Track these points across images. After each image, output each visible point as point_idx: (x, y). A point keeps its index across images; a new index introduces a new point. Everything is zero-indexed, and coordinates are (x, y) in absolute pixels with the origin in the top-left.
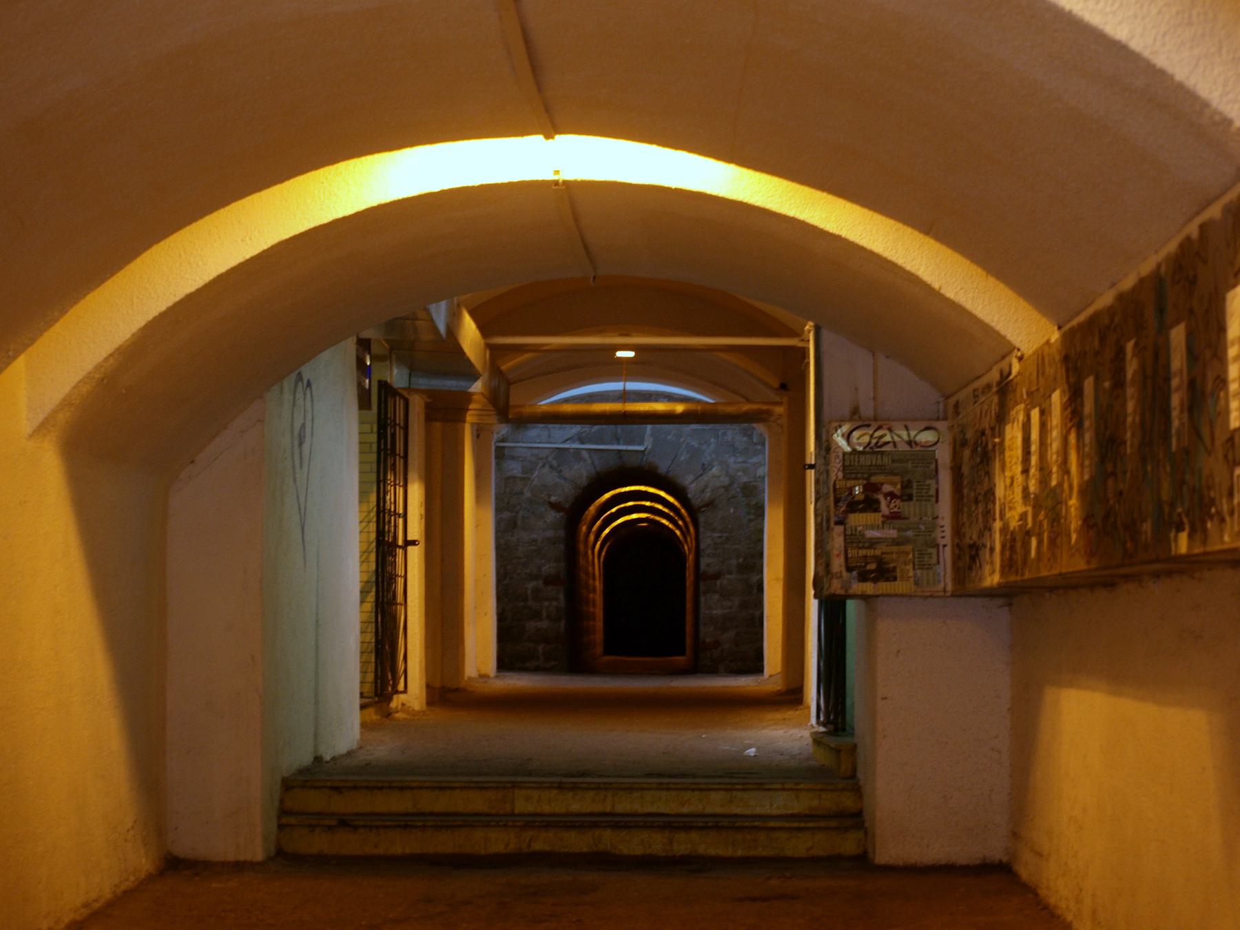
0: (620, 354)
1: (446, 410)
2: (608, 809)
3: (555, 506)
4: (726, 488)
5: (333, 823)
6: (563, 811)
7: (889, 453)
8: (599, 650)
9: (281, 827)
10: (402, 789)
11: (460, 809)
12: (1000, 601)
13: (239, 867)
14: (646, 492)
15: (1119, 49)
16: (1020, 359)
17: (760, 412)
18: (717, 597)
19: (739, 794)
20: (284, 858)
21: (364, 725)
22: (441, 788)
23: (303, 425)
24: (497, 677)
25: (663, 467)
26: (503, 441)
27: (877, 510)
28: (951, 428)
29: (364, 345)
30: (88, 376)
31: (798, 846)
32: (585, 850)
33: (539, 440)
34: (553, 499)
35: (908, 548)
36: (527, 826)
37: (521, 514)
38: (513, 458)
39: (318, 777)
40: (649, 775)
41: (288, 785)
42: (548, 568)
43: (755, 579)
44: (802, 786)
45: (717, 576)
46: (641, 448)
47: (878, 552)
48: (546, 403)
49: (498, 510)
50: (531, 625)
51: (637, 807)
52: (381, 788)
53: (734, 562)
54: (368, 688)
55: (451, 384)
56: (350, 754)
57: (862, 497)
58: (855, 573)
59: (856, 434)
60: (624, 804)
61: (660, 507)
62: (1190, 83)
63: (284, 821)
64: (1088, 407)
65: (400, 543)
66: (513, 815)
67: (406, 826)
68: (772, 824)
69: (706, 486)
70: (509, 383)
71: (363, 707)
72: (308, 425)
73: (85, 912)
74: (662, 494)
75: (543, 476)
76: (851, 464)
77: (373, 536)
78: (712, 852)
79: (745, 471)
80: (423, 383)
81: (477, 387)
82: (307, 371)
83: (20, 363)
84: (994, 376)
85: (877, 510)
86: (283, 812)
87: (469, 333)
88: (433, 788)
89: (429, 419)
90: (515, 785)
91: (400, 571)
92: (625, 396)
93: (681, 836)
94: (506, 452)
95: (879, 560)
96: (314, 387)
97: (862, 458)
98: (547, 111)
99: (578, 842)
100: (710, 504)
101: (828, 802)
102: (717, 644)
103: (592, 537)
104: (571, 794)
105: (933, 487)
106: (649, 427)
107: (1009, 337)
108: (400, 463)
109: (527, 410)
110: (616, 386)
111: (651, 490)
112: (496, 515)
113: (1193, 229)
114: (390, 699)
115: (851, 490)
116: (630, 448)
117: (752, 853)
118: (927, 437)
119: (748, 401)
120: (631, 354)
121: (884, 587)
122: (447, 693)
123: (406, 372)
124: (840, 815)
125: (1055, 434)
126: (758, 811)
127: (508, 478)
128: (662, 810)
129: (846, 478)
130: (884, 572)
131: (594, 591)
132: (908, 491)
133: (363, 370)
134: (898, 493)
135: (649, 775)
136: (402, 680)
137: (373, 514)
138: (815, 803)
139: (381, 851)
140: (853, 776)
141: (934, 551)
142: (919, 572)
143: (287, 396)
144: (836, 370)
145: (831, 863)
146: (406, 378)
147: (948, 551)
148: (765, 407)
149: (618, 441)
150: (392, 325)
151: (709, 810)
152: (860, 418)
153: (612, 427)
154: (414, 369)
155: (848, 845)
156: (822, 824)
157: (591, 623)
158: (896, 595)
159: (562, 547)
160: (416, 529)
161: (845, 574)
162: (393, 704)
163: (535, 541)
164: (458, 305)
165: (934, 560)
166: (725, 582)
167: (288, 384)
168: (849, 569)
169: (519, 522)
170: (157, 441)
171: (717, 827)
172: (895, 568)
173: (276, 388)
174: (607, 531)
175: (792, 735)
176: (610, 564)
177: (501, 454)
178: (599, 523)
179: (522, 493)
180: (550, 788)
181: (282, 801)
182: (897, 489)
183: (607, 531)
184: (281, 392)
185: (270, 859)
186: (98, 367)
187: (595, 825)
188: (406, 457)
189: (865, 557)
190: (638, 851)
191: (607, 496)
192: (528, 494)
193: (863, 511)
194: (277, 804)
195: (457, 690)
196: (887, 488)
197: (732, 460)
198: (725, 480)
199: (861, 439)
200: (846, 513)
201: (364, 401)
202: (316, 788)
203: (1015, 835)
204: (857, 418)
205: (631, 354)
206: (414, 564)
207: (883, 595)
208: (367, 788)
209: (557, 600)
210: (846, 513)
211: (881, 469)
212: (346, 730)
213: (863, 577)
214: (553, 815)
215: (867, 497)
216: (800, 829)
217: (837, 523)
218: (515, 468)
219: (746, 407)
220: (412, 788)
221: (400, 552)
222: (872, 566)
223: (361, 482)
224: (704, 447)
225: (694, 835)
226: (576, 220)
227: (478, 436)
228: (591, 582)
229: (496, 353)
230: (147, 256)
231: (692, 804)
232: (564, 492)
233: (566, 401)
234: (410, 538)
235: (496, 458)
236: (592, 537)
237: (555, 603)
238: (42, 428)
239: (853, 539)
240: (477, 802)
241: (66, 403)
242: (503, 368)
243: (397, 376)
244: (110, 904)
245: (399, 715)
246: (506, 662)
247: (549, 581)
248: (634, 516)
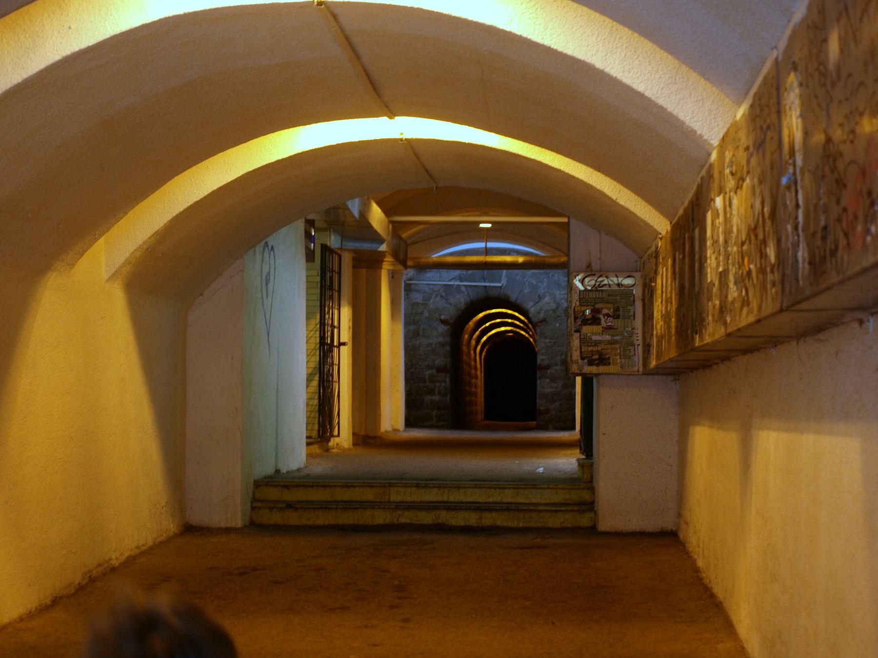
0: (482, 225)
1: (368, 263)
2: (445, 499)
3: (444, 322)
4: (554, 311)
5: (284, 506)
6: (419, 500)
7: (607, 291)
8: (481, 416)
9: (253, 508)
10: (324, 486)
11: (359, 499)
12: (672, 378)
13: (227, 531)
14: (506, 313)
15: (641, 95)
16: (661, 239)
19: (522, 491)
20: (254, 526)
21: (309, 455)
22: (347, 487)
23: (269, 274)
24: (405, 431)
25: (513, 297)
26: (410, 280)
27: (599, 324)
28: (642, 276)
29: (310, 223)
30: (139, 247)
31: (555, 521)
32: (431, 522)
34: (443, 317)
35: (617, 346)
36: (397, 508)
37: (422, 326)
38: (417, 291)
39: (277, 480)
40: (472, 480)
41: (257, 484)
42: (440, 362)
44: (559, 486)
45: (548, 367)
46: (500, 285)
47: (599, 349)
48: (436, 256)
49: (406, 324)
50: (428, 398)
51: (463, 498)
52: (312, 486)
53: (559, 358)
54: (314, 434)
55: (367, 246)
56: (298, 470)
57: (590, 316)
58: (586, 361)
59: (587, 280)
60: (455, 497)
61: (518, 323)
62: (675, 112)
63: (254, 505)
64: (677, 269)
65: (335, 344)
66: (390, 502)
67: (326, 508)
68: (540, 508)
69: (541, 310)
70: (407, 245)
71: (308, 444)
72: (272, 273)
73: (137, 551)
74: (517, 314)
75: (436, 302)
76: (584, 297)
77: (318, 340)
78: (505, 524)
80: (350, 245)
81: (383, 248)
82: (271, 241)
83: (102, 241)
84: (653, 249)
85: (599, 324)
86: (254, 500)
87: (376, 215)
88: (342, 487)
89: (355, 267)
90: (391, 485)
91: (336, 361)
92: (487, 252)
93: (487, 515)
95: (600, 353)
96: (276, 250)
97: (591, 293)
98: (386, 106)
99: (426, 518)
100: (543, 321)
101: (575, 496)
102: (547, 411)
103: (473, 342)
104: (423, 490)
105: (632, 311)
106: (505, 271)
107: (655, 227)
108: (336, 295)
109: (423, 261)
110: (481, 245)
111: (510, 312)
112: (405, 327)
113: (699, 180)
114: (329, 440)
115: (584, 312)
116: (492, 284)
117: (529, 525)
118: (628, 281)
120: (489, 225)
121: (602, 369)
122: (367, 438)
123: (339, 239)
124: (582, 503)
125: (669, 282)
126: (534, 501)
127: (414, 304)
128: (477, 500)
129: (581, 305)
130: (603, 360)
131: (476, 378)
132: (617, 313)
133: (308, 237)
134: (611, 314)
135: (472, 480)
136: (337, 429)
137: (318, 326)
138: (567, 497)
139: (311, 523)
140: (591, 481)
141: (632, 348)
142: (623, 361)
143: (258, 256)
144: (585, 243)
145: (575, 530)
146: (340, 241)
147: (640, 348)
149: (484, 280)
150: (328, 212)
151: (504, 500)
152: (592, 270)
153: (481, 271)
154: (344, 237)
155: (585, 520)
156: (570, 508)
157: (473, 399)
158: (609, 374)
159: (448, 348)
160: (346, 335)
161: (580, 361)
162: (331, 444)
163: (431, 344)
164: (368, 199)
165: (632, 353)
166: (553, 371)
167: (259, 249)
168: (583, 358)
169: (421, 332)
170: (184, 282)
171: (508, 510)
172: (609, 358)
173: (251, 251)
174: (485, 338)
175: (567, 462)
176: (489, 363)
177: (408, 288)
178: (477, 333)
179: (422, 313)
180: (411, 486)
181: (254, 494)
182: (611, 312)
183: (485, 338)
184: (255, 253)
185: (245, 526)
186: (145, 243)
187: (436, 508)
188: (339, 291)
189: (592, 351)
190: (462, 523)
191: (481, 315)
192: (426, 314)
193: (591, 324)
194: (251, 494)
195: (375, 437)
196: (605, 311)
197: (558, 292)
198: (553, 306)
199: (590, 282)
200: (581, 325)
201: (310, 256)
202: (274, 486)
203: (679, 515)
204: (590, 271)
205: (489, 225)
206: (344, 358)
207: (605, 374)
208: (304, 486)
210: (581, 325)
211: (602, 300)
212: (296, 456)
213: (591, 363)
214: (414, 502)
215: (593, 316)
216: (556, 511)
217: (575, 332)
218: (418, 297)
220: (330, 486)
221: (336, 350)
222: (596, 357)
223: (307, 306)
224: (540, 284)
225: (494, 514)
226: (418, 158)
227: (393, 277)
228: (473, 371)
229: (396, 228)
230: (173, 182)
231: (495, 497)
232: (450, 312)
233: (451, 254)
234: (342, 341)
235: (405, 290)
236: (473, 342)
237: (444, 384)
238: (113, 277)
239: (584, 341)
240: (369, 495)
241: (127, 262)
242: (404, 236)
243: (334, 241)
244: (151, 548)
245: (335, 451)
246: (410, 422)
247: (439, 370)
248: (503, 329)
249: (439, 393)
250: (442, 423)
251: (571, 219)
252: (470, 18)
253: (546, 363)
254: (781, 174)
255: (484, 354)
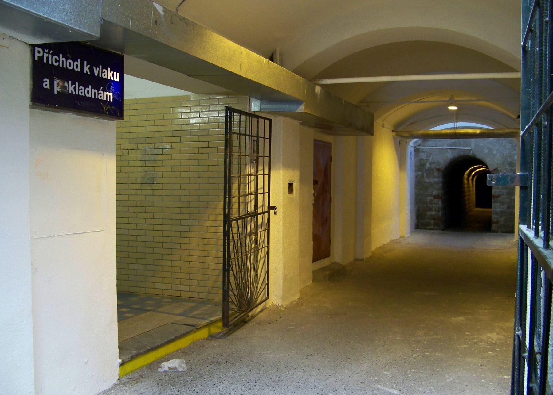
17: (513, 133)
18: (498, 204)
33: (432, 144)
38: (423, 152)
43: (512, 198)
45: (498, 197)
50: (429, 213)
79: (510, 157)
94: (420, 150)
102: (497, 222)
119: (508, 128)
148: (515, 131)
159: (441, 185)
192: (428, 165)
209: (438, 204)
218: (423, 156)
219: (507, 131)
227: (326, 220)
234: (271, 205)
247: (435, 197)
249: (435, 210)
251: (126, 76)
253: (497, 194)
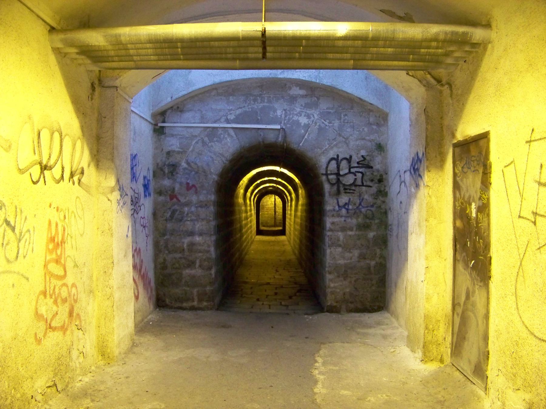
38: (172, 135)
50: (187, 272)
159: (212, 208)
178: (252, 188)
218: (173, 144)
250: (205, 304)
252: (241, 23)
254: (329, 113)
255: (256, 199)
